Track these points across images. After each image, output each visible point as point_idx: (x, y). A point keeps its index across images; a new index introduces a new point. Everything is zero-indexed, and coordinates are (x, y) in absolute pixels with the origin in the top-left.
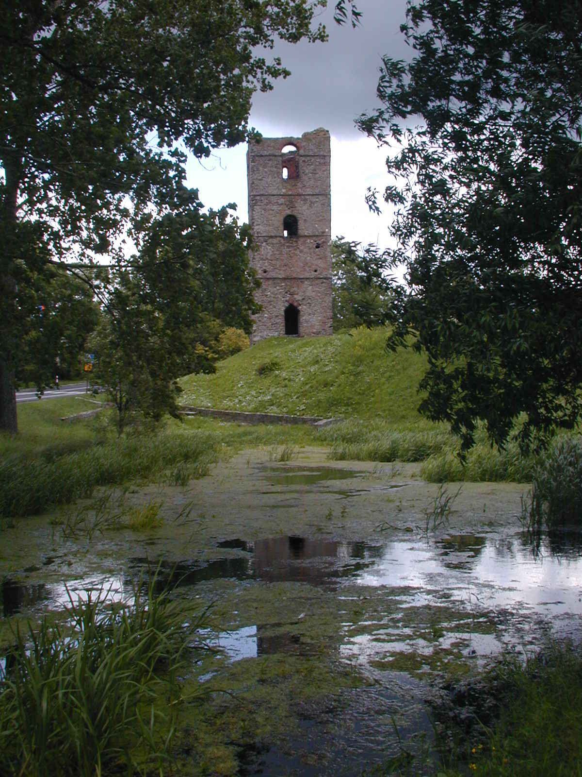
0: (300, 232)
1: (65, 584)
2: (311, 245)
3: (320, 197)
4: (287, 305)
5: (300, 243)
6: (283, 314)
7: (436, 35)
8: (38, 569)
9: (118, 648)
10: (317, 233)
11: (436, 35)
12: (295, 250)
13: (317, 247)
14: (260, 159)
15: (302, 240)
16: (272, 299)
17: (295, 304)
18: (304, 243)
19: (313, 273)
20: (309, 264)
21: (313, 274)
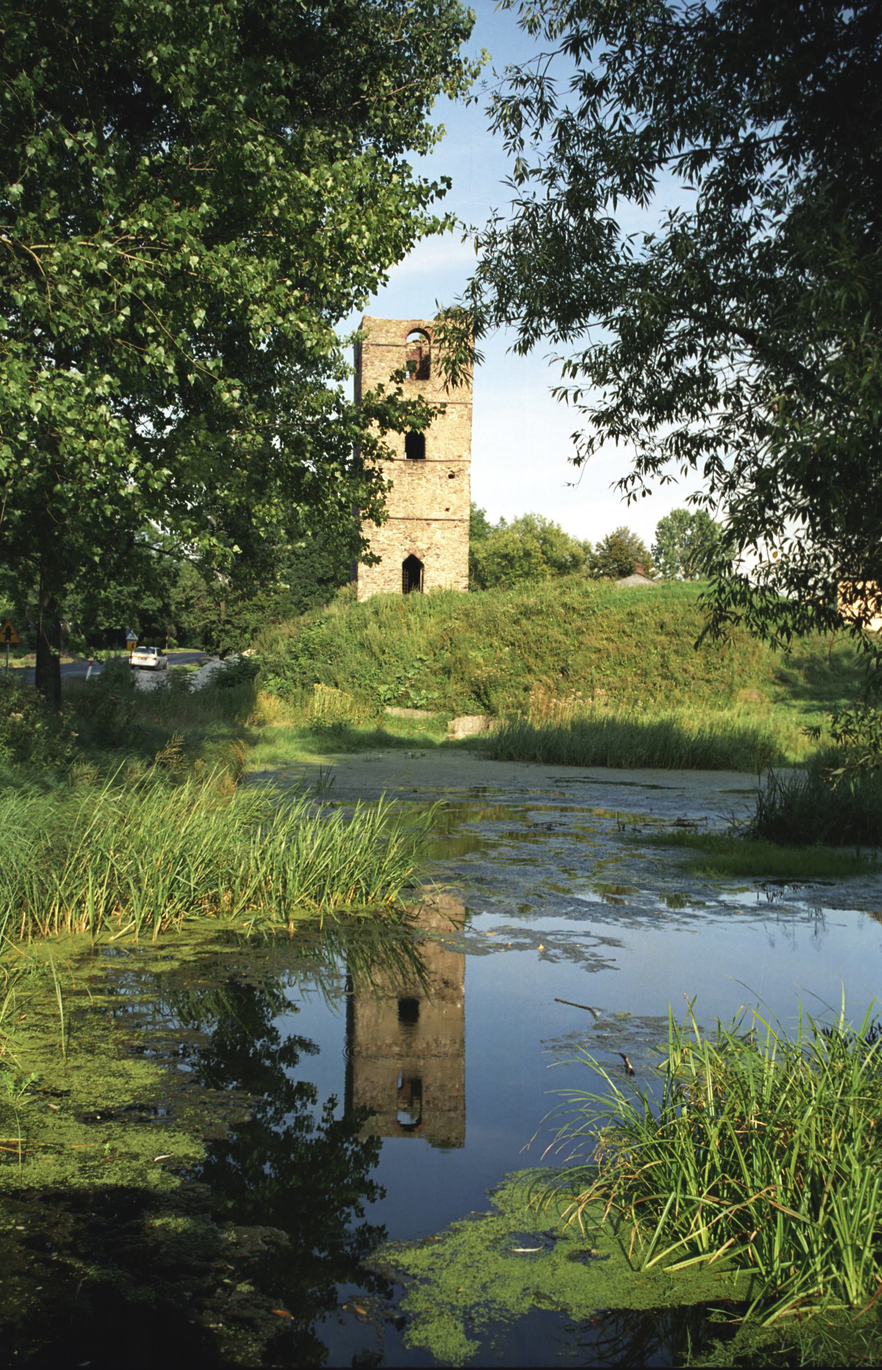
0: (428, 454)
1: (368, 1057)
2: (442, 474)
3: (457, 406)
4: (406, 555)
5: (427, 469)
6: (400, 567)
7: (17, 1049)
8: (538, 1180)
9: (134, 918)
10: (451, 458)
11: (17, 1049)
12: (419, 479)
13: (451, 477)
14: (376, 348)
15: (428, 463)
16: (386, 546)
17: (418, 555)
18: (433, 470)
19: (444, 512)
20: (439, 500)
21: (443, 515)
